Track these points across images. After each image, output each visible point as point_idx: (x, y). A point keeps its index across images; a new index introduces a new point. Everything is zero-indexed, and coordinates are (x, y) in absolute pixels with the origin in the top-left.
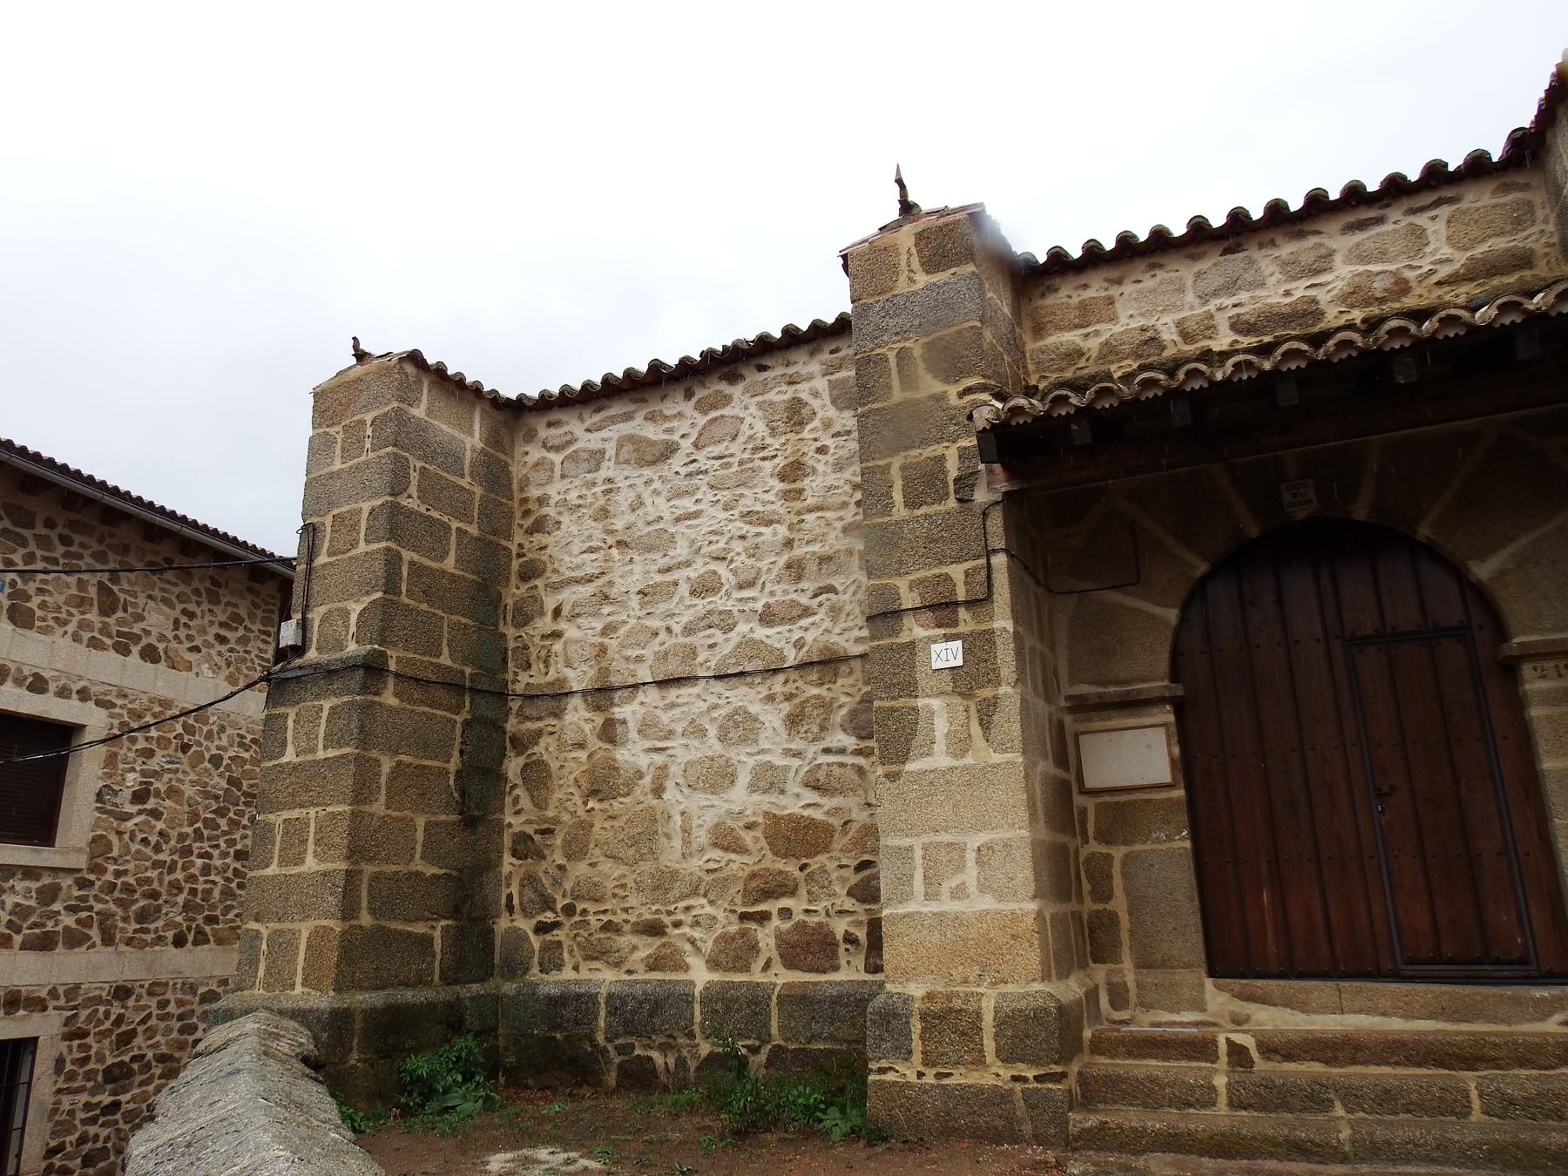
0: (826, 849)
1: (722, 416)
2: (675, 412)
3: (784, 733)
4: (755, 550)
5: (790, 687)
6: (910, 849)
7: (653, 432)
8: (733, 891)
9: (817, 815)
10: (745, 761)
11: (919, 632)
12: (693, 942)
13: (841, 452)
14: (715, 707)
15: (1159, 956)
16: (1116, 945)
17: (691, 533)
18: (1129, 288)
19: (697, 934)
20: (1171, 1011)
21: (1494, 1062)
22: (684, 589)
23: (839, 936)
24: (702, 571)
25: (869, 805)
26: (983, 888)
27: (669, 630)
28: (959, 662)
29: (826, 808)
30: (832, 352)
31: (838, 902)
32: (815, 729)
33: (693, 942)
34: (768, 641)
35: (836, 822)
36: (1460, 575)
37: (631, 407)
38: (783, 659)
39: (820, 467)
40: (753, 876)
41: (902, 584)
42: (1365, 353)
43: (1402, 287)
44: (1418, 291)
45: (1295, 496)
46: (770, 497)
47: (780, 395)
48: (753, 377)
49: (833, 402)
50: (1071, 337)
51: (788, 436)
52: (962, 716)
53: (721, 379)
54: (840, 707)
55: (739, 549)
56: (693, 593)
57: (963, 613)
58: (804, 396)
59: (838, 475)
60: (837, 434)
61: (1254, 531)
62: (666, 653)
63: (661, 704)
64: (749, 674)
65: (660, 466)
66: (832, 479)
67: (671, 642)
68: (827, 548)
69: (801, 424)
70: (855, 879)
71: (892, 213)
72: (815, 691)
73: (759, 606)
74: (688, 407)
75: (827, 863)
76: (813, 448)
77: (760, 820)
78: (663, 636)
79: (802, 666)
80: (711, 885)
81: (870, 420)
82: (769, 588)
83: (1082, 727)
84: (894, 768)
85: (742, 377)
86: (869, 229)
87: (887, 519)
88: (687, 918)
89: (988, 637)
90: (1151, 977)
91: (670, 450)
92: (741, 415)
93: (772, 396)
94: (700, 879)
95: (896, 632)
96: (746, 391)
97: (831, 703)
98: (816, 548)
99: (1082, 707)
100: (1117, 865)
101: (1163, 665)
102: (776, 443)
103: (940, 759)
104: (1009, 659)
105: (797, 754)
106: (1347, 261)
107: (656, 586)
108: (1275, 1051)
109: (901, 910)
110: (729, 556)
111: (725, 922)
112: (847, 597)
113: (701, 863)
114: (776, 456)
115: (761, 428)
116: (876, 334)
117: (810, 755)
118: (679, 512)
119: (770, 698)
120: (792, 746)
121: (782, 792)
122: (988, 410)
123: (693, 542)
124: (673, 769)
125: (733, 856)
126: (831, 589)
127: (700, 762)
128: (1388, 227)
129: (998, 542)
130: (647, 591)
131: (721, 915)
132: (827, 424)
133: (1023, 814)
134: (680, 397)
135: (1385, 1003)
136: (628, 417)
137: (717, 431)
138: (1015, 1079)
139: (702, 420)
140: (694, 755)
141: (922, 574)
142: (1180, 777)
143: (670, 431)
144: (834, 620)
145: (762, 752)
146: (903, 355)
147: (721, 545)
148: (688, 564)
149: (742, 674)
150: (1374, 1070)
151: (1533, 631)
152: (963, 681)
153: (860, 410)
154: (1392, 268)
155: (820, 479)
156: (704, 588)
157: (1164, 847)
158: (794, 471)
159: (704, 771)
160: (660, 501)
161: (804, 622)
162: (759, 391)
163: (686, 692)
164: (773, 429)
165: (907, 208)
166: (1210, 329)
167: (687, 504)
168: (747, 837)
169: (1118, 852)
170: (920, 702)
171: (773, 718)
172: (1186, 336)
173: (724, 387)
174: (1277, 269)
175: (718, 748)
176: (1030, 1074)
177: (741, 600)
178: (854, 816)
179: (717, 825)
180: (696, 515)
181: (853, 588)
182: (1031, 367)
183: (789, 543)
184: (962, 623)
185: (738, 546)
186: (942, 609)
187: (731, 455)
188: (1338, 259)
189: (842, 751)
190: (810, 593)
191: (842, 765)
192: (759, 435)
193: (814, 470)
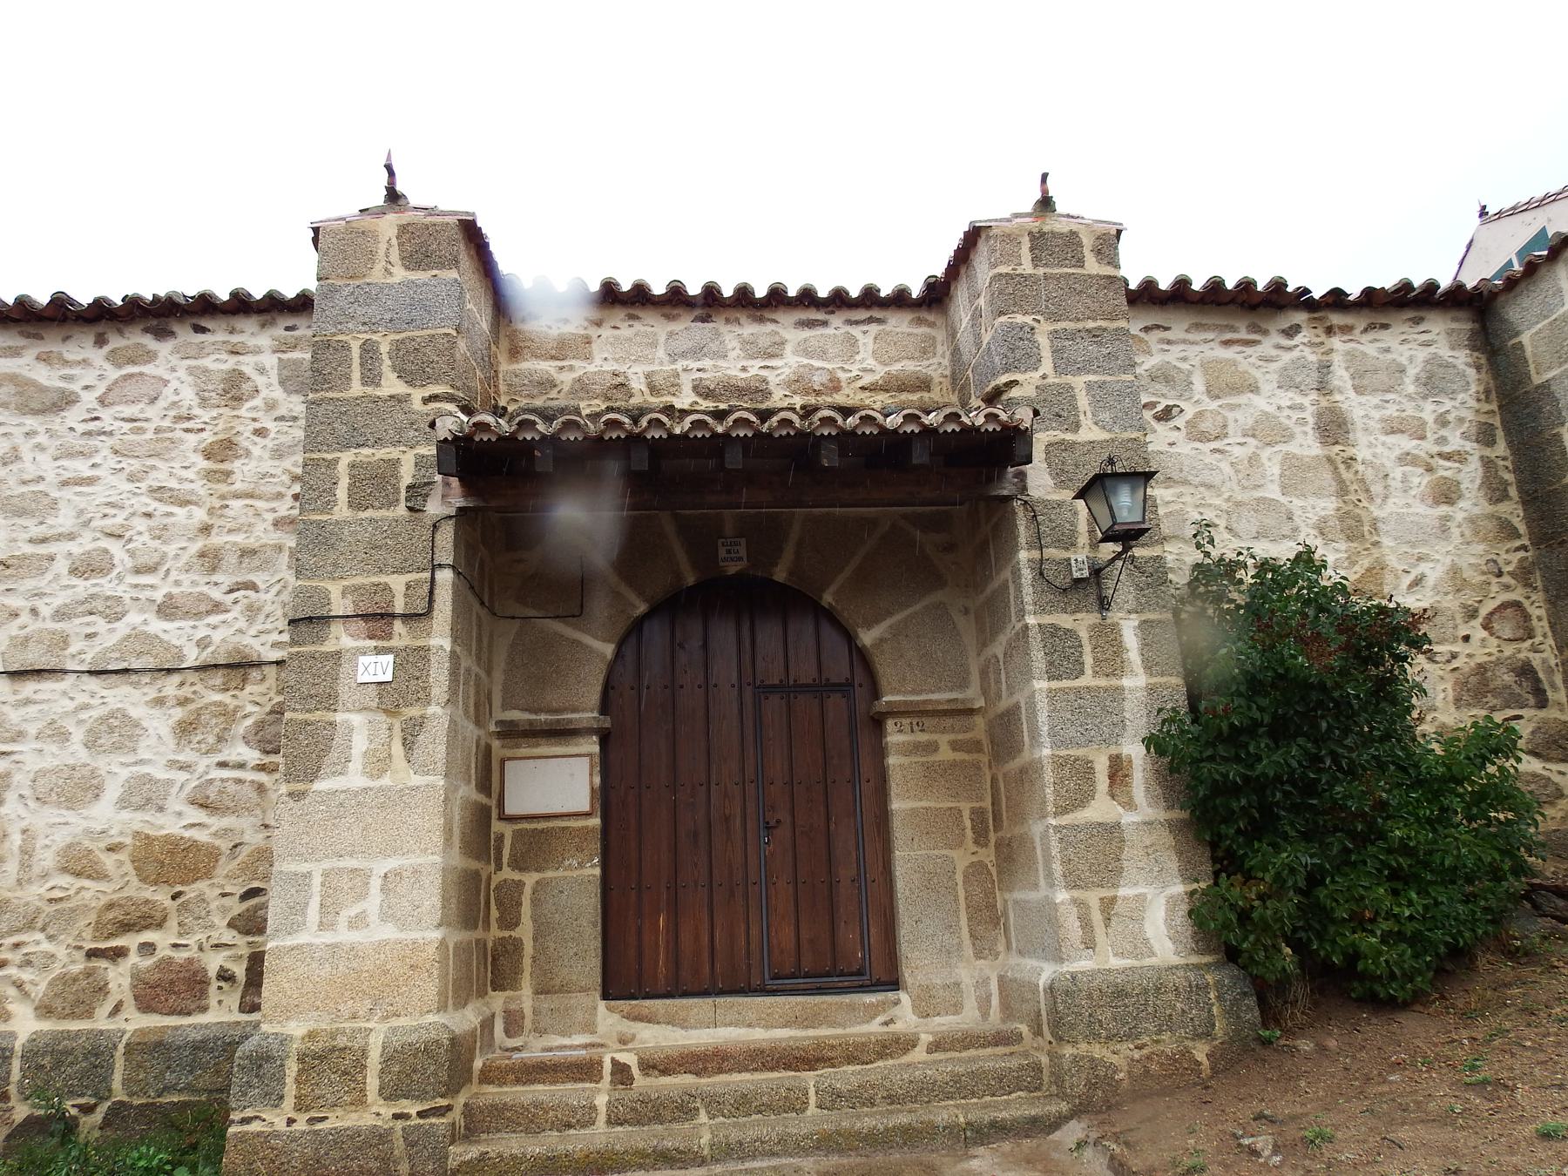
0: (208, 875)
1: (141, 374)
2: (80, 358)
3: (171, 742)
4: (161, 534)
5: (186, 691)
6: (308, 875)
7: (46, 376)
8: (82, 923)
9: (202, 836)
10: (117, 772)
11: (347, 642)
12: (19, 986)
13: (283, 439)
14: (86, 707)
15: (557, 982)
16: (517, 971)
17: (81, 502)
18: (606, 332)
19: (26, 975)
20: (563, 1034)
21: (829, 1062)
22: (61, 566)
23: (212, 972)
24: (89, 547)
25: (266, 826)
26: (385, 917)
27: (34, 612)
28: (388, 677)
29: (213, 829)
30: (287, 329)
31: (215, 934)
32: (211, 739)
33: (19, 986)
34: (165, 637)
35: (224, 845)
36: (850, 638)
37: (19, 342)
38: (181, 658)
39: (256, 451)
40: (110, 906)
41: (335, 589)
42: (801, 434)
43: (835, 386)
44: (846, 391)
45: (729, 552)
46: (190, 474)
47: (218, 364)
48: (185, 335)
49: (282, 383)
50: (546, 367)
51: (221, 411)
52: (384, 734)
53: (146, 330)
54: (245, 716)
55: (142, 528)
56: (74, 571)
57: (398, 626)
58: (248, 370)
59: (277, 463)
60: (281, 419)
61: (690, 580)
62: (27, 639)
63: (12, 699)
64: (136, 671)
65: (49, 417)
66: (268, 465)
67: (34, 626)
68: (252, 540)
69: (238, 399)
70: (238, 908)
71: (378, 198)
72: (218, 697)
73: (159, 596)
74: (97, 356)
75: (207, 891)
76: (251, 428)
77: (128, 841)
78: (25, 618)
79: (203, 668)
80: (55, 917)
81: (321, 410)
82: (174, 575)
83: (509, 753)
84: (300, 786)
85: (172, 334)
86: (350, 209)
87: (325, 517)
88: (16, 957)
89: (423, 653)
90: (547, 1003)
91: (65, 401)
92: (166, 377)
93: (208, 362)
94: (38, 911)
95: (321, 640)
96: (176, 351)
97: (235, 711)
98: (239, 538)
99: (510, 732)
100: (528, 891)
101: (594, 697)
102: (206, 415)
103: (355, 778)
104: (442, 678)
105: (185, 767)
106: (796, 352)
107: (25, 557)
108: (654, 1067)
109: (289, 942)
110: (128, 535)
111: (66, 960)
112: (269, 596)
113: (42, 891)
114: (202, 430)
115: (188, 396)
116: (340, 319)
117: (201, 769)
118: (67, 475)
119: (159, 702)
120: (181, 758)
121: (161, 809)
122: (452, 422)
123: (81, 512)
124: (17, 778)
125: (87, 883)
126: (253, 586)
127: (55, 771)
128: (829, 331)
129: (446, 554)
130: (9, 562)
131: (61, 952)
132: (271, 406)
133: (438, 838)
134: (89, 340)
135: (752, 1016)
136: (15, 352)
137: (131, 389)
138: (396, 1117)
139: (114, 374)
140: (48, 763)
141: (359, 580)
142: (598, 806)
143: (68, 378)
144: (251, 620)
145: (141, 762)
146: (369, 350)
147: (119, 520)
148: (71, 537)
149: (126, 671)
150: (736, 1077)
151: (899, 692)
152: (389, 698)
153: (311, 396)
154: (829, 366)
155: (253, 464)
156: (86, 568)
157: (575, 874)
158: (223, 450)
159: (61, 782)
160: (45, 460)
161: (214, 619)
162: (193, 353)
163: (47, 687)
164: (203, 399)
165: (393, 196)
166: (674, 388)
167: (81, 467)
168: (109, 861)
169: (530, 879)
170: (339, 717)
171: (159, 725)
172: (653, 389)
173: (149, 341)
174: (738, 346)
175: (83, 755)
176: (413, 1112)
177: (136, 586)
178: (246, 838)
179: (69, 846)
180: (91, 481)
181: (277, 587)
182: (503, 388)
183: (206, 529)
184: (396, 637)
185: (140, 524)
186: (377, 619)
187: (146, 420)
188: (789, 348)
189: (241, 766)
190: (225, 588)
191: (239, 781)
192: (186, 403)
193: (248, 453)
